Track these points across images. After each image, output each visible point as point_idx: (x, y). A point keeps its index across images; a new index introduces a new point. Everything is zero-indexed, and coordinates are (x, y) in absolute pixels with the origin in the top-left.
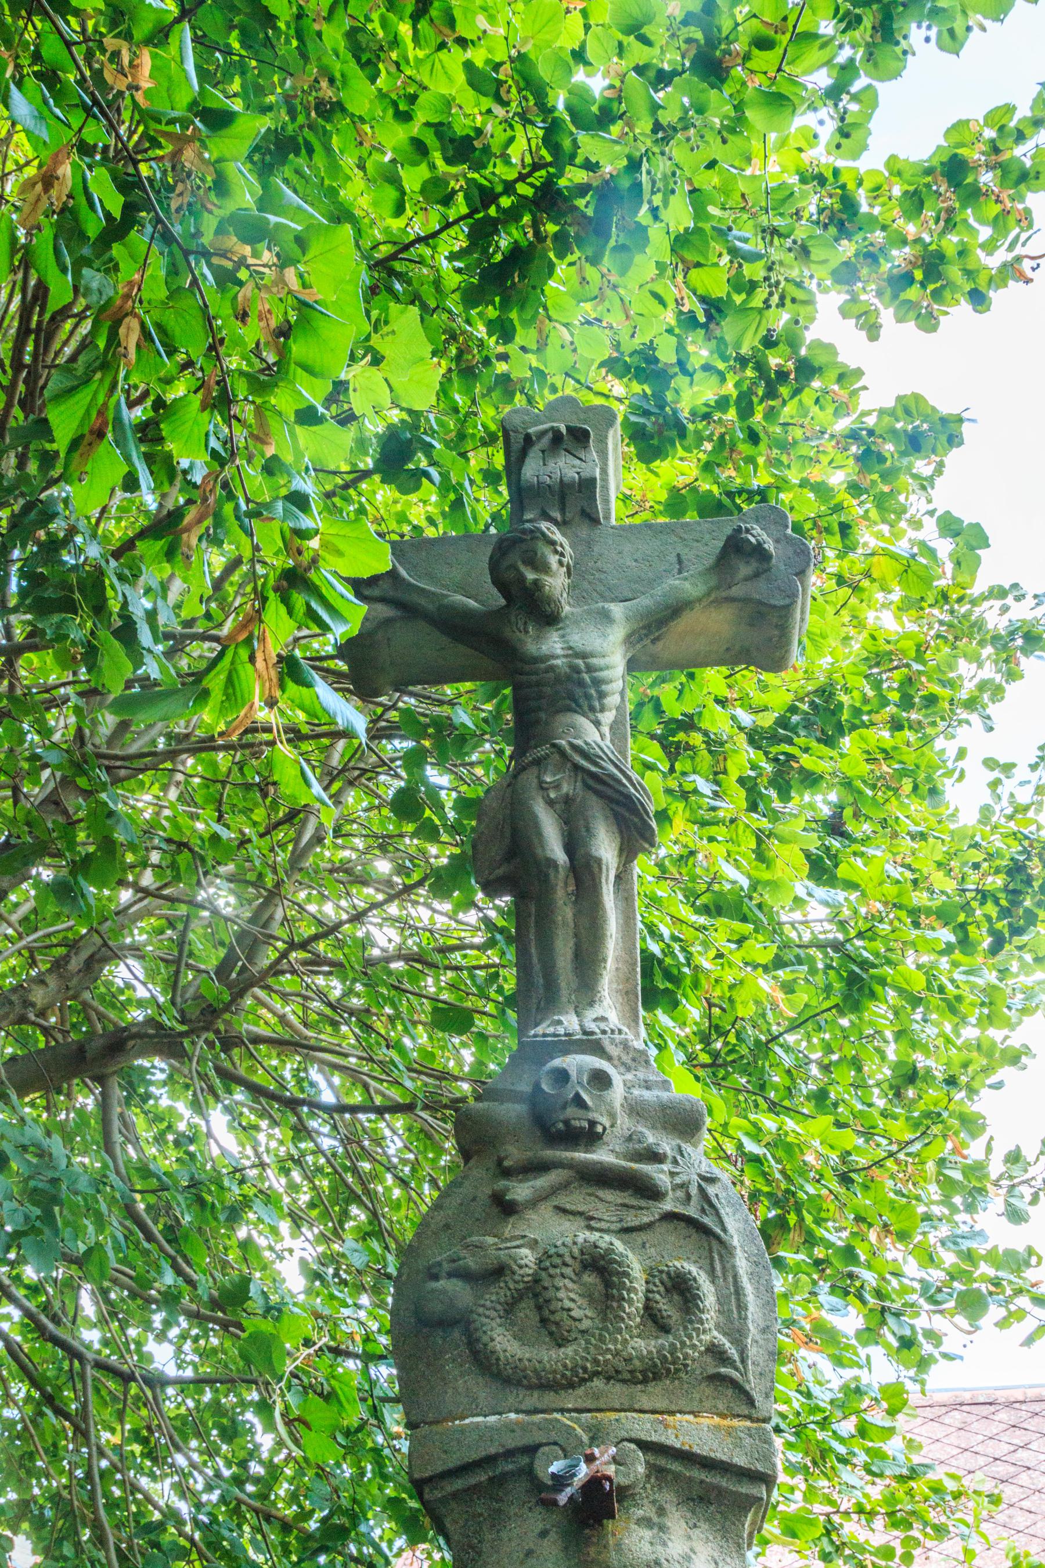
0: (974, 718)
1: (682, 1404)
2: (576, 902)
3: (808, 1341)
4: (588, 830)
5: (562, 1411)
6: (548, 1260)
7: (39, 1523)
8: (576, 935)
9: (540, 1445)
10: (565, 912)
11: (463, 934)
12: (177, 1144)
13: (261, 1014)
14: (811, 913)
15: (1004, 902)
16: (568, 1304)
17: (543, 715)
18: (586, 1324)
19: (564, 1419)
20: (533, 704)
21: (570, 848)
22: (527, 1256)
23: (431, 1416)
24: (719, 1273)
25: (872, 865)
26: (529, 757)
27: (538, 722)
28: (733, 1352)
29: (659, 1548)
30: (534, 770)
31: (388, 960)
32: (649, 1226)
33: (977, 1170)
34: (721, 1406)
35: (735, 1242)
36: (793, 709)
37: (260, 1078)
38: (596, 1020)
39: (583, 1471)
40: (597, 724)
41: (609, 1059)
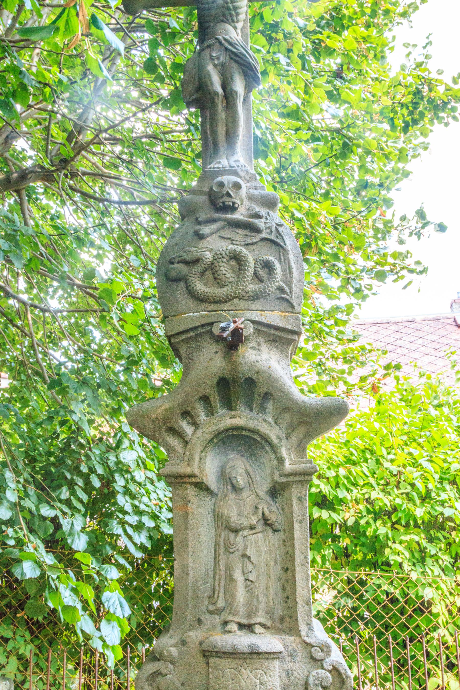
0: (404, 21)
1: (268, 308)
2: (226, 111)
3: (317, 290)
4: (231, 78)
5: (222, 310)
6: (217, 256)
7: (11, 369)
8: (226, 125)
9: (214, 322)
10: (222, 114)
11: (171, 126)
12: (52, 219)
13: (83, 164)
14: (326, 115)
15: (411, 108)
16: (224, 272)
17: (211, 24)
18: (231, 279)
19: (223, 313)
20: (207, 18)
21: (224, 87)
22: (209, 255)
23: (173, 314)
24: (283, 260)
25: (355, 91)
26: (206, 44)
27: (209, 27)
28: (287, 289)
30: (207, 51)
31: (141, 138)
32: (256, 243)
33: (387, 223)
34: (282, 309)
35: (289, 249)
36: (322, 18)
37: (86, 189)
38: (235, 161)
39: (232, 326)
40: (235, 28)
41: (240, 177)
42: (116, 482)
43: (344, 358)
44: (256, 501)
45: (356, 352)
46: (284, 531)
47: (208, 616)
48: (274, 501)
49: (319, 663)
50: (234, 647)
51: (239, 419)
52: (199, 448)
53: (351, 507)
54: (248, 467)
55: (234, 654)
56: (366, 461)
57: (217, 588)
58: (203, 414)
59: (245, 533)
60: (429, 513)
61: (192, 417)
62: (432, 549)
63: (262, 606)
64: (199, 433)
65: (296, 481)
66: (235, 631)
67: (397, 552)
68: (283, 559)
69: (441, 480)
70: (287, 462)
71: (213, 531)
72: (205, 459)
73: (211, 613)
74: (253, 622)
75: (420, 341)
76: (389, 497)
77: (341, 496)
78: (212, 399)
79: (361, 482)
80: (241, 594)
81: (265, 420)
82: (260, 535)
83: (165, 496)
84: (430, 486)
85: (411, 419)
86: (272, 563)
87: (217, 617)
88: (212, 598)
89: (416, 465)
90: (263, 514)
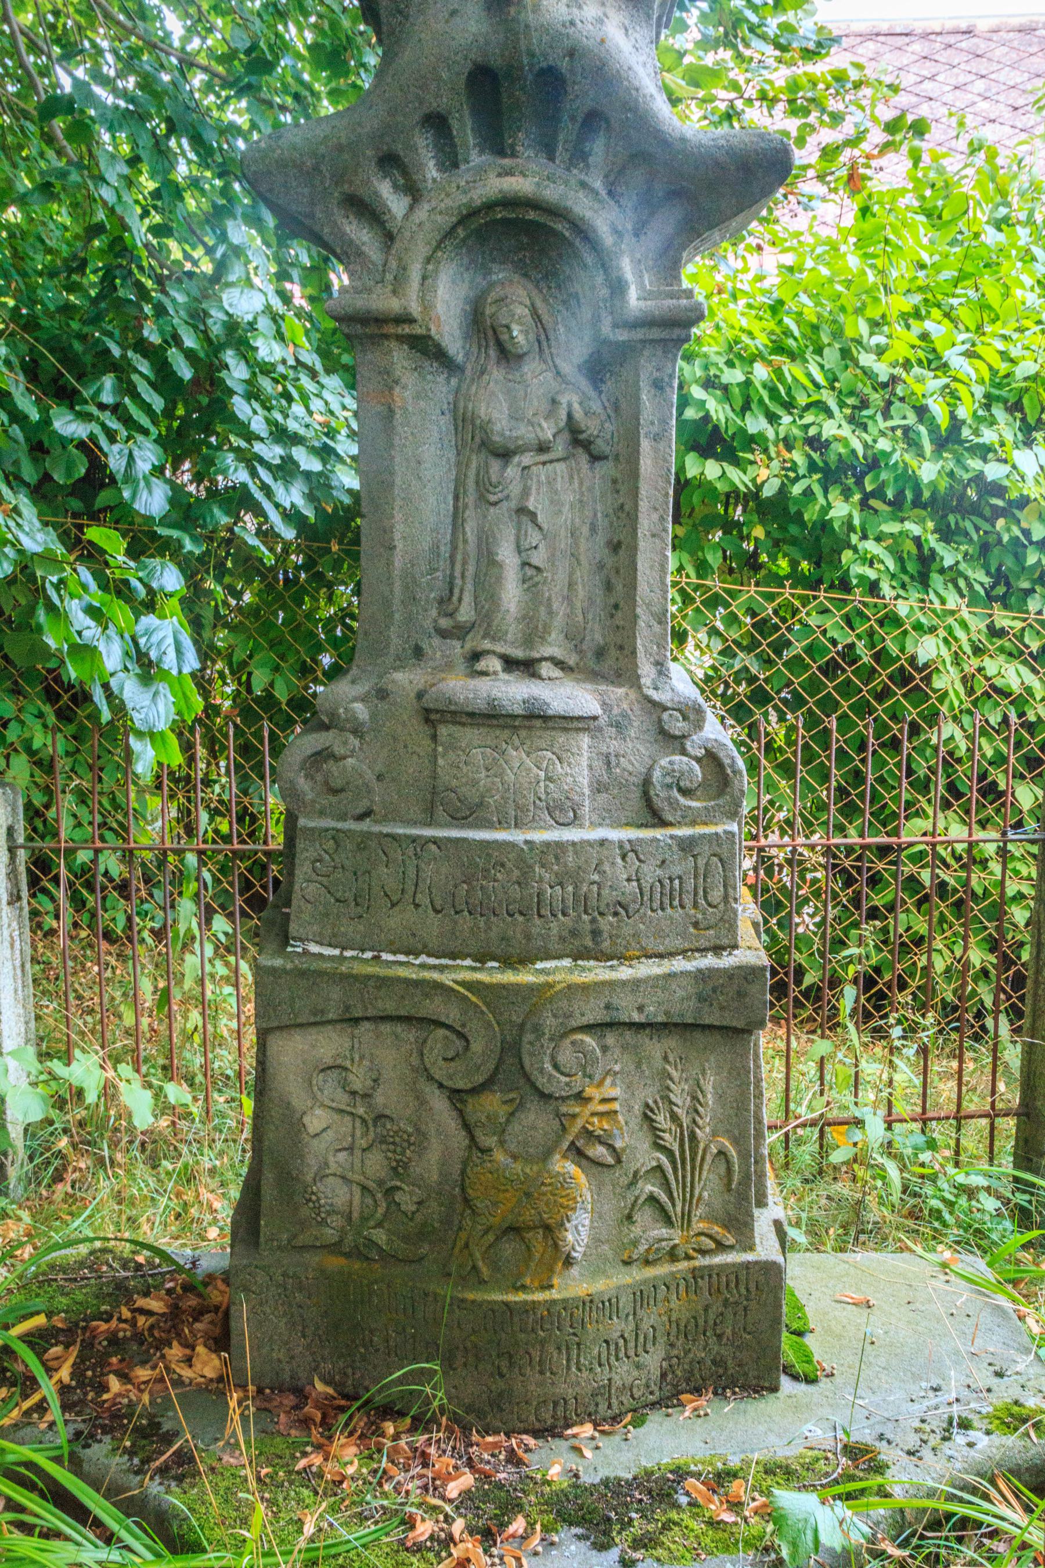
29: (575, 11)
42: (227, 367)
43: (791, 101)
44: (554, 385)
45: (821, 86)
46: (617, 457)
47: (436, 641)
48: (596, 388)
49: (677, 743)
50: (491, 702)
51: (521, 180)
52: (422, 250)
53: (773, 455)
54: (539, 304)
55: (494, 716)
56: (819, 351)
57: (458, 582)
58: (431, 164)
59: (527, 459)
60: (951, 474)
61: (405, 173)
62: (948, 557)
63: (559, 621)
64: (422, 213)
65: (652, 341)
66: (495, 673)
67: (869, 559)
68: (611, 524)
69: (989, 401)
70: (633, 294)
71: (452, 455)
72: (435, 279)
73: (444, 634)
74: (537, 656)
75: (980, 85)
76: (864, 435)
77: (752, 430)
78: (455, 124)
79: (802, 400)
80: (511, 595)
81: (583, 185)
82: (560, 467)
83: (344, 408)
84: (962, 413)
85: (936, 257)
86: (585, 530)
87: (457, 644)
88: (446, 602)
89: (936, 363)
90: (570, 416)
